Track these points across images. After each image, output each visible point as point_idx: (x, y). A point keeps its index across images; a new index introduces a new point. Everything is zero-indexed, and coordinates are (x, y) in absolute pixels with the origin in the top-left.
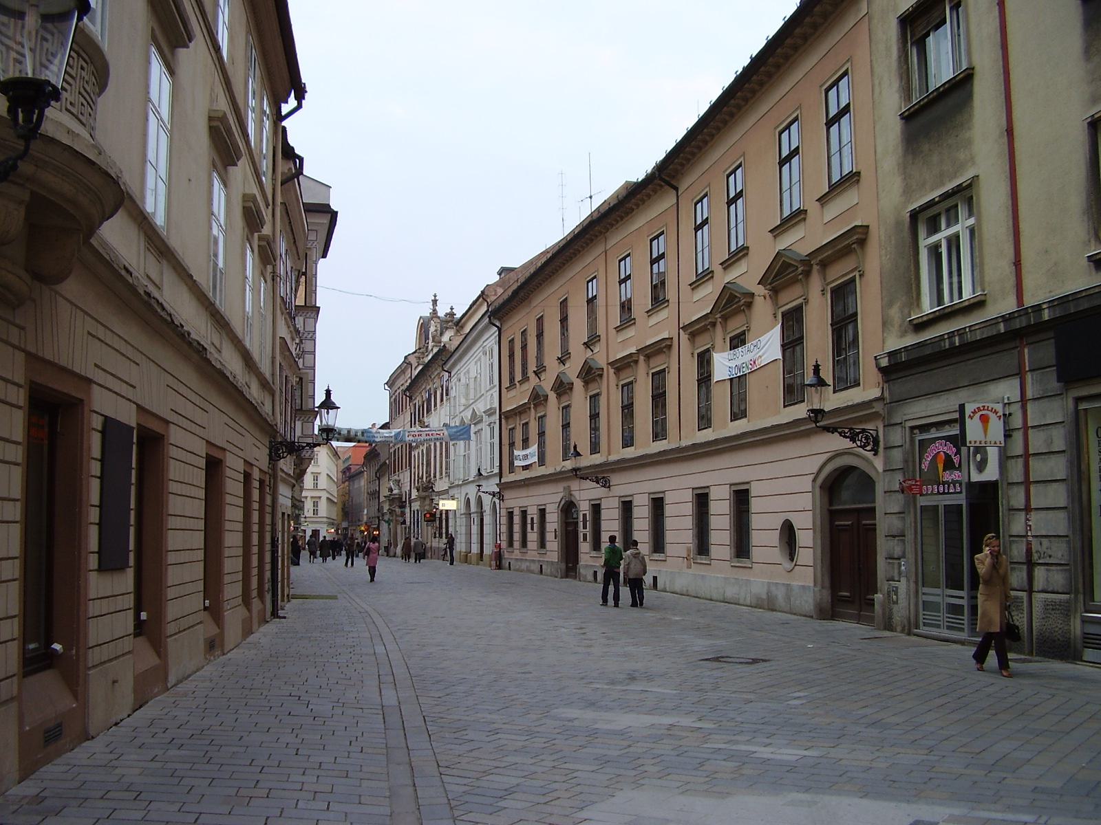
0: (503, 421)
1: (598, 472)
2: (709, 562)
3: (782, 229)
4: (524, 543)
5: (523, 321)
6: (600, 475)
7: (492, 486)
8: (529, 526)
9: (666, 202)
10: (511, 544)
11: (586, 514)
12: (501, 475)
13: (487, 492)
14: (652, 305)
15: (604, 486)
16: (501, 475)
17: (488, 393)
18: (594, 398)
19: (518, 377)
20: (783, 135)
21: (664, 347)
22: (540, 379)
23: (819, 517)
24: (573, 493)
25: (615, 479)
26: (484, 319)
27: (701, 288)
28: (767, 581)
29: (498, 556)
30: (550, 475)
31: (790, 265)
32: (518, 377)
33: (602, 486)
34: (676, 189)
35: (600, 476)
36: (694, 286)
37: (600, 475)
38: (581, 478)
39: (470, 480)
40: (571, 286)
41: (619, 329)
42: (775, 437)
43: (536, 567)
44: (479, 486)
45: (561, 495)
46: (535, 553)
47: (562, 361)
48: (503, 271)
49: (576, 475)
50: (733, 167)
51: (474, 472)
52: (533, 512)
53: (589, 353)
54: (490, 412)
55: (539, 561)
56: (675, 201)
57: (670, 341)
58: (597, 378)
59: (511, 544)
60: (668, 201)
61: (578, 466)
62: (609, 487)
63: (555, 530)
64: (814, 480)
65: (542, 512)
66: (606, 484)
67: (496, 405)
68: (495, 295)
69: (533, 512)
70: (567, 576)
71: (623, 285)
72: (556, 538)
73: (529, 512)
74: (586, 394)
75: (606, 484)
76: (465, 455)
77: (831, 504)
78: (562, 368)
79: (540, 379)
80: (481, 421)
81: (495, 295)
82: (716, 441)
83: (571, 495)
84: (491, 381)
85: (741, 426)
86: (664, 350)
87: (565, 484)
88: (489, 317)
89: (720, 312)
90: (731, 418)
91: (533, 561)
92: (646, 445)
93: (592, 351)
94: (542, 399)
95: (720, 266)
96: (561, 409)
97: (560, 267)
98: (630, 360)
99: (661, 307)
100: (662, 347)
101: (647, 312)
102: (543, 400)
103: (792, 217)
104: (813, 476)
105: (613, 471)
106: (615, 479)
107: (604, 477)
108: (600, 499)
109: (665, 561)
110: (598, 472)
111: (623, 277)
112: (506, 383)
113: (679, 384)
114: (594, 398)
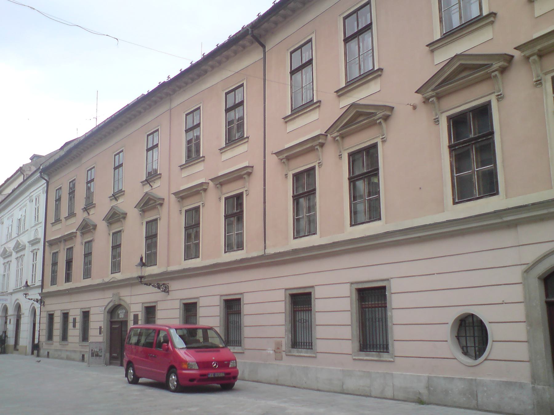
0: (47, 247)
1: (161, 280)
2: (314, 355)
3: (449, 40)
4: (64, 337)
5: (62, 180)
6: (162, 283)
7: (35, 294)
8: (70, 325)
9: (253, 57)
10: (50, 337)
11: (138, 315)
12: (42, 287)
13: (32, 299)
14: (226, 144)
15: (164, 291)
16: (42, 287)
17: (33, 229)
18: (116, 235)
19: (64, 212)
20: (149, 137)
21: (245, 174)
22: (89, 214)
23: (354, 315)
24: (122, 298)
25: (174, 285)
26: (36, 174)
27: (297, 120)
28: (427, 375)
29: (36, 347)
30: (98, 285)
31: (117, 214)
32: (64, 212)
33: (162, 291)
34: (263, 46)
35: (161, 283)
36: (341, 93)
37: (162, 283)
38: (145, 284)
39: (36, 285)
40: (101, 158)
41: (182, 167)
42: (340, 250)
43: (79, 356)
44: (26, 294)
45: (109, 300)
46: (58, 344)
47: (115, 197)
48: (35, 158)
49: (141, 281)
50: (152, 131)
51: (24, 283)
52: (75, 314)
53: (85, 215)
54: (34, 242)
55: (81, 352)
56: (262, 56)
57: (251, 168)
58: (159, 207)
59: (50, 337)
60: (256, 56)
61: (143, 275)
62: (168, 292)
63: (100, 328)
64: (105, 309)
65: (86, 315)
66: (166, 290)
67: (41, 235)
68: (30, 170)
69: (75, 314)
70: (110, 364)
71: (117, 171)
72: (100, 333)
73: (70, 314)
74: (109, 230)
75: (166, 290)
76: (4, 275)
77: (547, 296)
78: (114, 203)
79: (89, 214)
80: (24, 249)
81: (30, 170)
82: (242, 261)
83: (120, 299)
84: (37, 217)
85: (88, 282)
86: (244, 176)
87: (115, 291)
88: (41, 173)
89: (338, 131)
90: (225, 250)
91: (75, 351)
92: (78, 281)
93: (152, 187)
94: (91, 228)
95: (428, 48)
96: (84, 243)
97: (59, 168)
98: (199, 189)
99: (306, 111)
100: (70, 237)
101: (220, 150)
102: (93, 229)
103: (452, 33)
104: (524, 267)
105: (172, 279)
106: (174, 285)
107: (164, 284)
108: (156, 302)
109: (243, 353)
110: (161, 280)
111: (117, 165)
112: (51, 219)
113: (265, 202)
114: (116, 235)
